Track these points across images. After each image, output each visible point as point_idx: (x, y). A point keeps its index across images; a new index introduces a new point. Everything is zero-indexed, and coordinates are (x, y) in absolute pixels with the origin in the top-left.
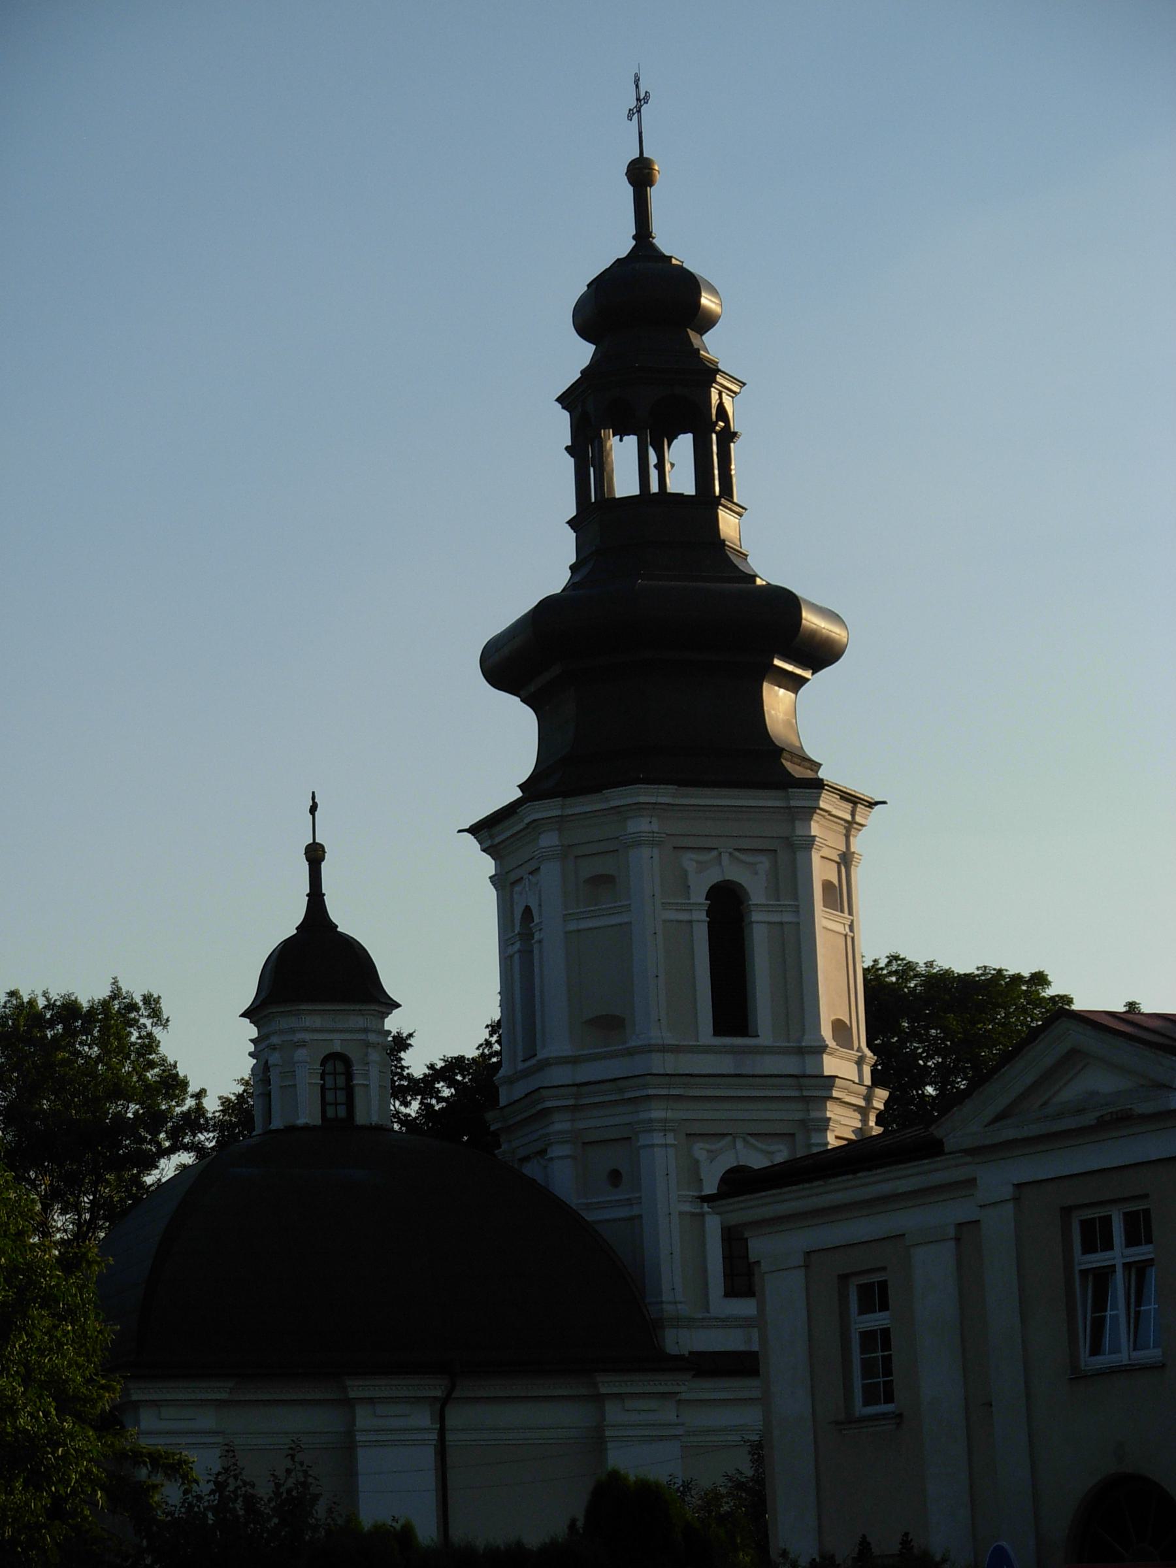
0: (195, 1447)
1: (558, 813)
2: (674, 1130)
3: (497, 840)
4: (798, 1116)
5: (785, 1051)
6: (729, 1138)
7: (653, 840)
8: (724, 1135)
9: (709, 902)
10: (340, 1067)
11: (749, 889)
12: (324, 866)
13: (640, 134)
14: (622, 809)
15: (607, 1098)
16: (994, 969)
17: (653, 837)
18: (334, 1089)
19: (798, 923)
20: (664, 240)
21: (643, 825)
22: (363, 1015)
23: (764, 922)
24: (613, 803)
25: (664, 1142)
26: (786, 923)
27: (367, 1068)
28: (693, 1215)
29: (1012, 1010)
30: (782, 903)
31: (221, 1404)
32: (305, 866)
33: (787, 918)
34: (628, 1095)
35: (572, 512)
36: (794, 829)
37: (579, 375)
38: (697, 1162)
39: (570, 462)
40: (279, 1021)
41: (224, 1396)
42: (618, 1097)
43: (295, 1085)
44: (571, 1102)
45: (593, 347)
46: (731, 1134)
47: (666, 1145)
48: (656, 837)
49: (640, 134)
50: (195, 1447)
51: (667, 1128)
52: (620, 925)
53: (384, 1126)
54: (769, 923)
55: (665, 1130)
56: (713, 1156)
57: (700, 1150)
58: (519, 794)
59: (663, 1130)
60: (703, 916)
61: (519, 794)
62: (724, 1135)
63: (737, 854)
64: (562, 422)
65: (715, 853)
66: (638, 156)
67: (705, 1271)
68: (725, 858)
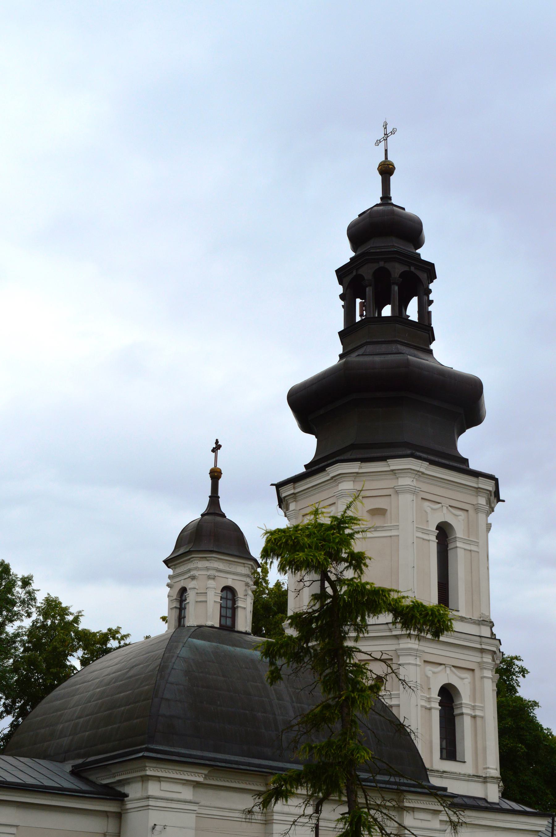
1: (292, 491)
2: (420, 657)
3: (361, 471)
4: (479, 660)
6: (443, 667)
7: (415, 489)
8: (441, 664)
9: (438, 531)
10: (230, 596)
12: (220, 481)
13: (386, 151)
14: (396, 472)
17: (415, 489)
18: (227, 607)
21: (405, 481)
22: (245, 567)
23: (463, 548)
24: (392, 468)
25: (415, 663)
26: (474, 551)
27: (245, 598)
28: (426, 708)
30: (470, 539)
31: (197, 785)
32: (209, 481)
35: (342, 328)
37: (349, 261)
38: (428, 678)
40: (197, 563)
41: (200, 779)
43: (206, 601)
45: (390, 306)
46: (444, 664)
47: (416, 665)
48: (417, 490)
49: (386, 151)
51: (417, 655)
52: (391, 536)
53: (248, 632)
54: (465, 549)
55: (416, 656)
58: (304, 470)
59: (414, 655)
60: (434, 538)
61: (304, 470)
62: (441, 664)
63: (450, 508)
65: (440, 505)
66: (383, 159)
68: (445, 508)
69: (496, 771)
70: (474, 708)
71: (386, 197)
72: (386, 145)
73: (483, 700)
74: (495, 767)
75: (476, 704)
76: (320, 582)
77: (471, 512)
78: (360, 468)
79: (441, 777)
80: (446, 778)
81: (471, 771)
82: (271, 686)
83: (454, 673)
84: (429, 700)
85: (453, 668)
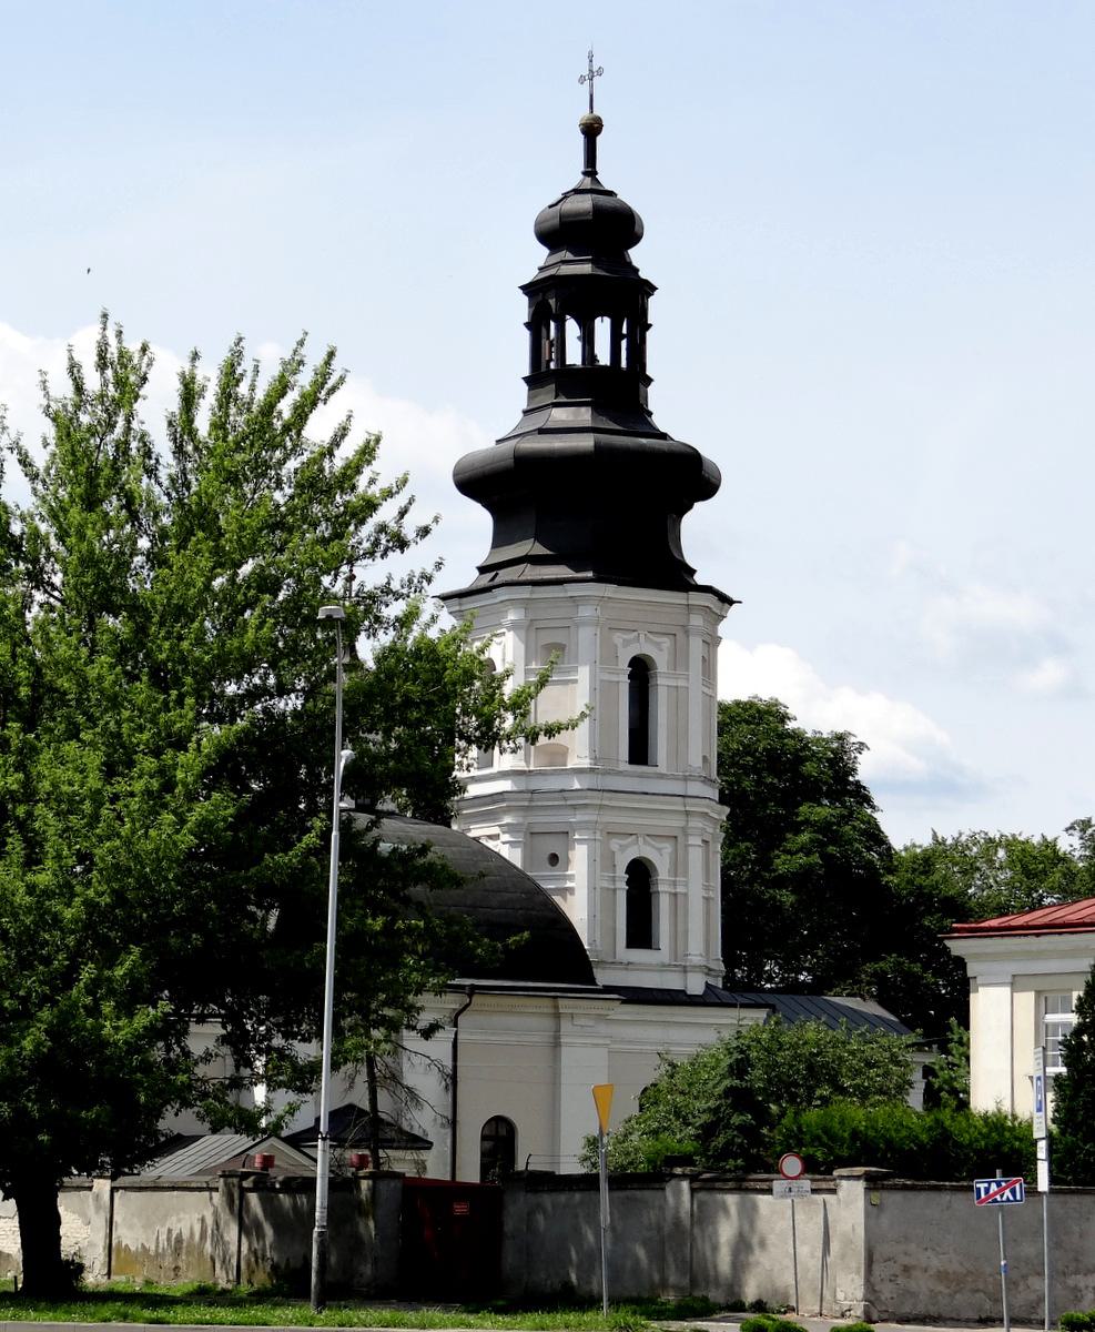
0: (640, 607)
1: (528, 596)
3: (534, 596)
5: (675, 778)
6: (634, 837)
11: (656, 661)
13: (591, 96)
15: (556, 803)
16: (920, 846)
19: (687, 688)
20: (606, 179)
24: (570, 594)
29: (1080, 1118)
33: (681, 683)
34: (569, 803)
36: (689, 620)
39: (526, 334)
42: (563, 803)
44: (526, 804)
45: (608, 364)
49: (591, 96)
50: (640, 607)
56: (623, 848)
57: (615, 844)
64: (521, 308)
65: (636, 633)
66: (575, 177)
67: (615, 929)
69: (700, 958)
70: (675, 884)
71: (590, 168)
72: (592, 86)
73: (686, 874)
74: (698, 953)
75: (678, 890)
76: (448, 1178)
77: (680, 636)
78: (532, 593)
79: (627, 969)
80: (632, 970)
81: (667, 961)
82: (422, 1008)
83: (650, 844)
84: (614, 879)
85: (647, 838)
